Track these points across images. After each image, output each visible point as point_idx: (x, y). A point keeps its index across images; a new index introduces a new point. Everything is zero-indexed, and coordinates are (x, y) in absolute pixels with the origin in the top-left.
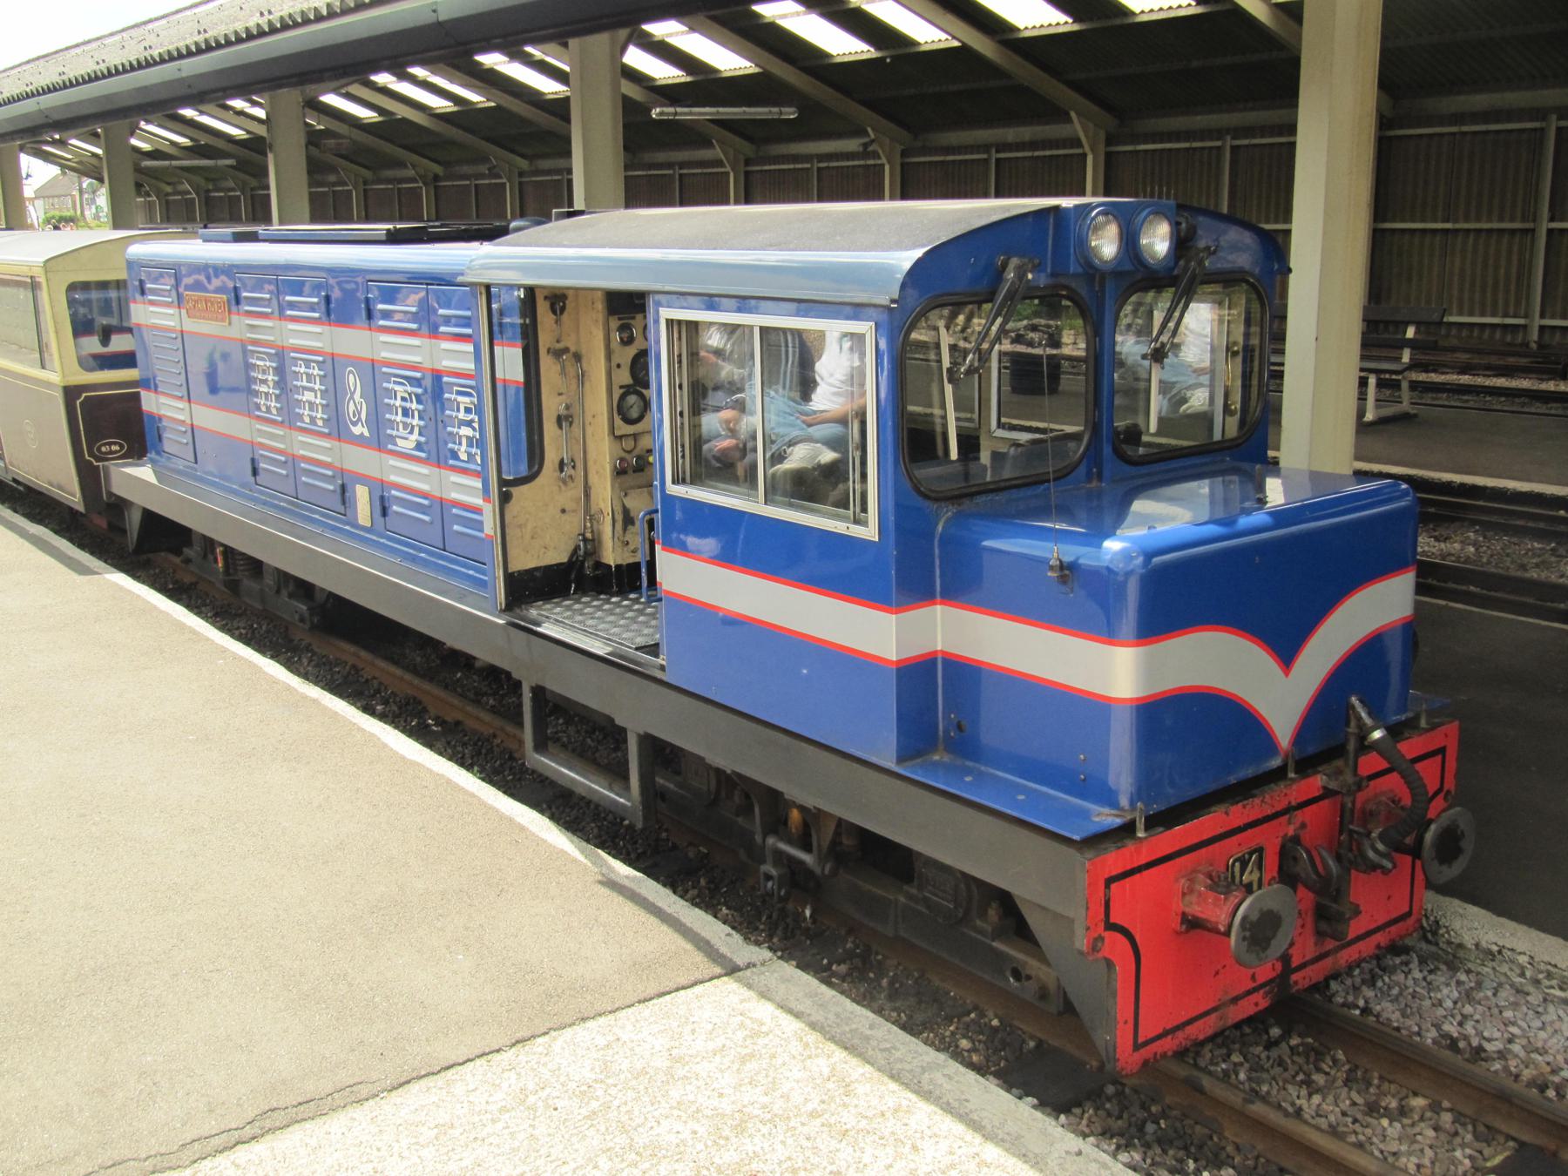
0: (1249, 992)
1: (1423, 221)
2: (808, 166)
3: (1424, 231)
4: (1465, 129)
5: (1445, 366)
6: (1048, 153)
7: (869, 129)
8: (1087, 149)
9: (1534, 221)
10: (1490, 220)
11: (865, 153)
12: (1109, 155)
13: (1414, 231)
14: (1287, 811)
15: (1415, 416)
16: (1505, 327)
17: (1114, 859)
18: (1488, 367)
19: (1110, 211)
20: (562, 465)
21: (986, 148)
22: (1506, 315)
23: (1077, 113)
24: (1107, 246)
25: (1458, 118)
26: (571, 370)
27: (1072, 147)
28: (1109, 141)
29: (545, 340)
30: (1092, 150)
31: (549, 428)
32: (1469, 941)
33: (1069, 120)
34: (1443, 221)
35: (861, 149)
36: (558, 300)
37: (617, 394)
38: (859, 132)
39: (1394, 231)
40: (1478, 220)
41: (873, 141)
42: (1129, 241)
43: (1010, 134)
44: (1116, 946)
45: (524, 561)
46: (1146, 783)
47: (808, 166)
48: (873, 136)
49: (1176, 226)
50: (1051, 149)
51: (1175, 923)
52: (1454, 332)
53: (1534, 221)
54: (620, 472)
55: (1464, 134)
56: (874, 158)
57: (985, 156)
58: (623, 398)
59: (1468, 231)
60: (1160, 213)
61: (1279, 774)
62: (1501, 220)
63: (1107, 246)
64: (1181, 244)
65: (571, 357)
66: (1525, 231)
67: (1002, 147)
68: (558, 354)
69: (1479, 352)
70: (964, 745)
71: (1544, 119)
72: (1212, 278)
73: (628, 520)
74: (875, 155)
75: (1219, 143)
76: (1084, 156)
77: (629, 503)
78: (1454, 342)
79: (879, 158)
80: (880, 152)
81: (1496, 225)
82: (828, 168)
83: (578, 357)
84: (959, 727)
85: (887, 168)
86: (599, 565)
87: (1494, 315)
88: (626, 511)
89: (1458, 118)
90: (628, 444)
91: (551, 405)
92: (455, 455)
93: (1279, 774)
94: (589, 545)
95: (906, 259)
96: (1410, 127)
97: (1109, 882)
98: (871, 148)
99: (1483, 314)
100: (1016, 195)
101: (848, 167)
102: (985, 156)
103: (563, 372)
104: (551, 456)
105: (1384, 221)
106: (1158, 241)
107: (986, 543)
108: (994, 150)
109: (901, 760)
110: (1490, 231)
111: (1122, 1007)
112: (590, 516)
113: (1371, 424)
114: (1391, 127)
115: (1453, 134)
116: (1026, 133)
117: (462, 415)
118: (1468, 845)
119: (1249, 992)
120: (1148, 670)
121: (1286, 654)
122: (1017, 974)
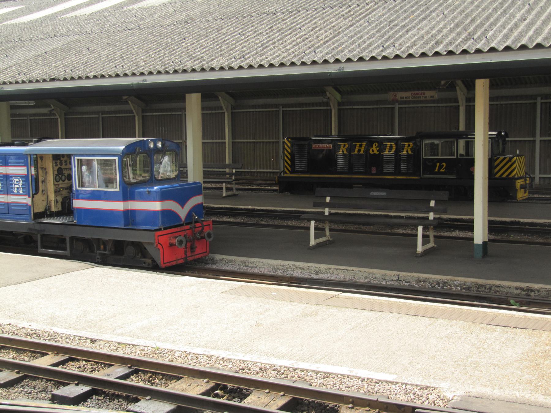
0: (181, 259)
1: (247, 139)
2: (26, 118)
3: (247, 142)
4: (256, 110)
5: (253, 184)
6: (121, 115)
7: (52, 105)
8: (135, 114)
9: (279, 139)
10: (266, 139)
11: (51, 113)
12: (143, 116)
13: (244, 142)
14: (184, 230)
15: (238, 195)
16: (274, 172)
17: (159, 233)
18: (265, 184)
19: (152, 140)
20: (43, 191)
21: (97, 113)
22: (274, 169)
23: (131, 102)
24: (152, 146)
25: (254, 107)
26: (44, 172)
27: (130, 113)
28: (143, 111)
29: (39, 165)
30: (137, 114)
31: (40, 184)
32: (218, 259)
33: (128, 104)
34: (253, 139)
35: (49, 112)
36: (42, 157)
37: (55, 176)
38: (48, 106)
39: (238, 142)
40: (263, 139)
41: (53, 110)
42: (155, 145)
43: (106, 108)
44: (159, 246)
45: (36, 211)
46: (163, 223)
47: (26, 118)
48: (53, 107)
49: (162, 142)
50: (122, 114)
51: (169, 245)
52: (259, 175)
53: (279, 139)
54: (55, 192)
55: (256, 112)
56: (53, 116)
57: (98, 116)
58: (56, 177)
59: (260, 142)
60: (160, 140)
61: (182, 225)
62: (269, 139)
63: (152, 146)
64: (163, 145)
65: (44, 169)
66: (277, 142)
67: (103, 113)
68: (42, 168)
69: (265, 180)
70: (134, 223)
71: (278, 108)
72: (168, 151)
73: (57, 202)
74: (54, 115)
75: (180, 113)
76: (135, 116)
77: (57, 198)
78: (259, 178)
79: (56, 116)
80: (56, 114)
81: (252, 141)
82: (34, 119)
83: (45, 169)
84: (133, 221)
85: (59, 120)
86: (51, 212)
87: (270, 169)
88: (57, 200)
89: (254, 107)
90: (57, 186)
91: (41, 179)
92: (13, 192)
93: (182, 225)
94: (48, 208)
95: (122, 148)
96: (240, 109)
97: (158, 236)
98: (53, 112)
99: (267, 169)
100: (128, 137)
101: (43, 119)
102: (98, 116)
103: (43, 172)
104: (41, 189)
105: (235, 139)
106: (160, 145)
107: (136, 190)
108: (101, 114)
109: (124, 226)
110: (267, 142)
111: (161, 257)
112: (48, 202)
113: (225, 197)
114: (235, 109)
115: (253, 112)
116: (113, 108)
117: (15, 183)
118: (212, 236)
119: (181, 259)
120: (162, 206)
121: (182, 205)
122: (145, 263)
